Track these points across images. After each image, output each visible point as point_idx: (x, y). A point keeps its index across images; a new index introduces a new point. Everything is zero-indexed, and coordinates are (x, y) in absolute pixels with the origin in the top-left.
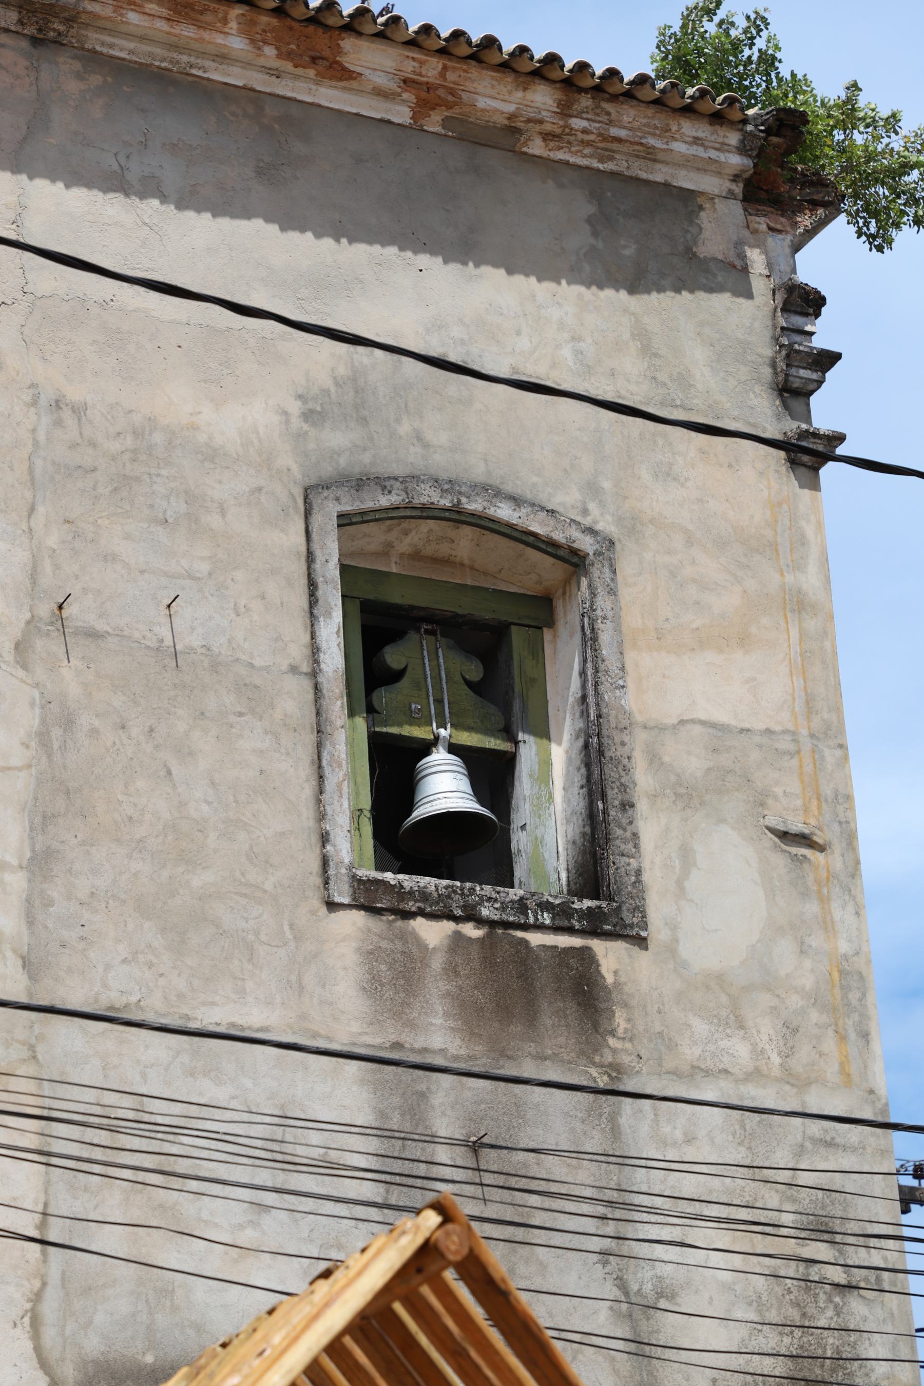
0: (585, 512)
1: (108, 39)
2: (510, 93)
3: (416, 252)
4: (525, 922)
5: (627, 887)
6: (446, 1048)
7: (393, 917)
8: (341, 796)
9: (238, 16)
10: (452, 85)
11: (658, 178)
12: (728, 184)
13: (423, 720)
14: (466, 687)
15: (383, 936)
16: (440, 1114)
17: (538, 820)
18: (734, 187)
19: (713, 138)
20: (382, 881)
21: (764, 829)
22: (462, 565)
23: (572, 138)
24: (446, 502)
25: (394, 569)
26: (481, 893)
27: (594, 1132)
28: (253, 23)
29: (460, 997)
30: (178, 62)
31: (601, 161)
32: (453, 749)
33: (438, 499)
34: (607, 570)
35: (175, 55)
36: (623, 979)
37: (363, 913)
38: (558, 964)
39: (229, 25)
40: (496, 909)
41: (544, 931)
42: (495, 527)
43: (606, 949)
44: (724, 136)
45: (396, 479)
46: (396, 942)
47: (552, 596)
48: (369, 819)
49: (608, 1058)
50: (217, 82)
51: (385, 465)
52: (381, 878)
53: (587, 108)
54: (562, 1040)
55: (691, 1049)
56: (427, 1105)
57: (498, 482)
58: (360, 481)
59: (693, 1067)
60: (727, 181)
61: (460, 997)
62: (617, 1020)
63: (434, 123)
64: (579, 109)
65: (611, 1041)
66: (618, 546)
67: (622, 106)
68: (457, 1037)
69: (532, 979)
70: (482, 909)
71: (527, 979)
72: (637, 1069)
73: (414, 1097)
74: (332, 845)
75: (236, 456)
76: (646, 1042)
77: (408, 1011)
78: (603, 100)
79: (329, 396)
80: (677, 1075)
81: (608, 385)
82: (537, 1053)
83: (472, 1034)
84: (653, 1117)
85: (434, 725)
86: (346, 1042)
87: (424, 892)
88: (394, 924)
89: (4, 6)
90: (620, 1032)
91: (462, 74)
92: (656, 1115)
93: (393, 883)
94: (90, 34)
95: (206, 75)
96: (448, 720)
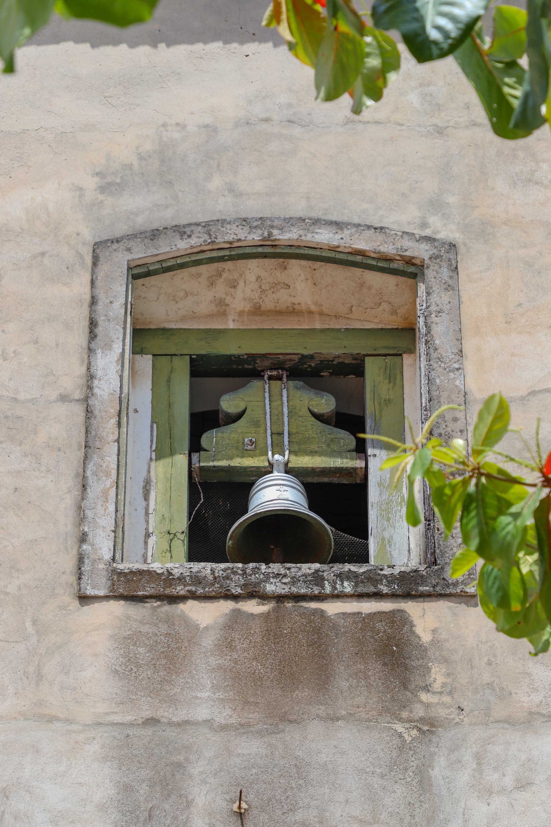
0: (424, 225)
3: (242, 43)
4: (320, 593)
5: (452, 549)
6: (213, 719)
7: (159, 603)
8: (107, 501)
13: (258, 451)
14: (313, 419)
15: (145, 621)
16: (199, 782)
17: (386, 523)
20: (148, 571)
22: (310, 312)
24: (256, 237)
25: (231, 326)
26: (267, 571)
27: (396, 786)
29: (234, 670)
32: (288, 471)
33: (246, 235)
34: (446, 270)
36: (444, 635)
37: (122, 602)
38: (361, 629)
40: (285, 584)
41: (346, 600)
42: (318, 253)
43: (424, 610)
45: (198, 224)
46: (160, 626)
48: (183, 541)
49: (419, 712)
51: (189, 216)
52: (146, 569)
54: (360, 700)
55: (529, 696)
56: (183, 774)
57: (320, 214)
58: (156, 232)
59: (531, 713)
61: (234, 670)
62: (433, 676)
65: (424, 696)
66: (462, 249)
68: (227, 707)
69: (326, 646)
70: (267, 585)
71: (320, 646)
72: (457, 720)
73: (168, 768)
74: (89, 544)
75: (20, 230)
76: (470, 694)
77: (168, 688)
79: (131, 169)
80: (509, 723)
81: (461, 117)
82: (327, 714)
83: (247, 703)
84: (475, 766)
85: (270, 453)
86: (89, 723)
87: (196, 577)
88: (159, 610)
90: (437, 687)
92: (478, 764)
93: (159, 571)
96: (287, 447)
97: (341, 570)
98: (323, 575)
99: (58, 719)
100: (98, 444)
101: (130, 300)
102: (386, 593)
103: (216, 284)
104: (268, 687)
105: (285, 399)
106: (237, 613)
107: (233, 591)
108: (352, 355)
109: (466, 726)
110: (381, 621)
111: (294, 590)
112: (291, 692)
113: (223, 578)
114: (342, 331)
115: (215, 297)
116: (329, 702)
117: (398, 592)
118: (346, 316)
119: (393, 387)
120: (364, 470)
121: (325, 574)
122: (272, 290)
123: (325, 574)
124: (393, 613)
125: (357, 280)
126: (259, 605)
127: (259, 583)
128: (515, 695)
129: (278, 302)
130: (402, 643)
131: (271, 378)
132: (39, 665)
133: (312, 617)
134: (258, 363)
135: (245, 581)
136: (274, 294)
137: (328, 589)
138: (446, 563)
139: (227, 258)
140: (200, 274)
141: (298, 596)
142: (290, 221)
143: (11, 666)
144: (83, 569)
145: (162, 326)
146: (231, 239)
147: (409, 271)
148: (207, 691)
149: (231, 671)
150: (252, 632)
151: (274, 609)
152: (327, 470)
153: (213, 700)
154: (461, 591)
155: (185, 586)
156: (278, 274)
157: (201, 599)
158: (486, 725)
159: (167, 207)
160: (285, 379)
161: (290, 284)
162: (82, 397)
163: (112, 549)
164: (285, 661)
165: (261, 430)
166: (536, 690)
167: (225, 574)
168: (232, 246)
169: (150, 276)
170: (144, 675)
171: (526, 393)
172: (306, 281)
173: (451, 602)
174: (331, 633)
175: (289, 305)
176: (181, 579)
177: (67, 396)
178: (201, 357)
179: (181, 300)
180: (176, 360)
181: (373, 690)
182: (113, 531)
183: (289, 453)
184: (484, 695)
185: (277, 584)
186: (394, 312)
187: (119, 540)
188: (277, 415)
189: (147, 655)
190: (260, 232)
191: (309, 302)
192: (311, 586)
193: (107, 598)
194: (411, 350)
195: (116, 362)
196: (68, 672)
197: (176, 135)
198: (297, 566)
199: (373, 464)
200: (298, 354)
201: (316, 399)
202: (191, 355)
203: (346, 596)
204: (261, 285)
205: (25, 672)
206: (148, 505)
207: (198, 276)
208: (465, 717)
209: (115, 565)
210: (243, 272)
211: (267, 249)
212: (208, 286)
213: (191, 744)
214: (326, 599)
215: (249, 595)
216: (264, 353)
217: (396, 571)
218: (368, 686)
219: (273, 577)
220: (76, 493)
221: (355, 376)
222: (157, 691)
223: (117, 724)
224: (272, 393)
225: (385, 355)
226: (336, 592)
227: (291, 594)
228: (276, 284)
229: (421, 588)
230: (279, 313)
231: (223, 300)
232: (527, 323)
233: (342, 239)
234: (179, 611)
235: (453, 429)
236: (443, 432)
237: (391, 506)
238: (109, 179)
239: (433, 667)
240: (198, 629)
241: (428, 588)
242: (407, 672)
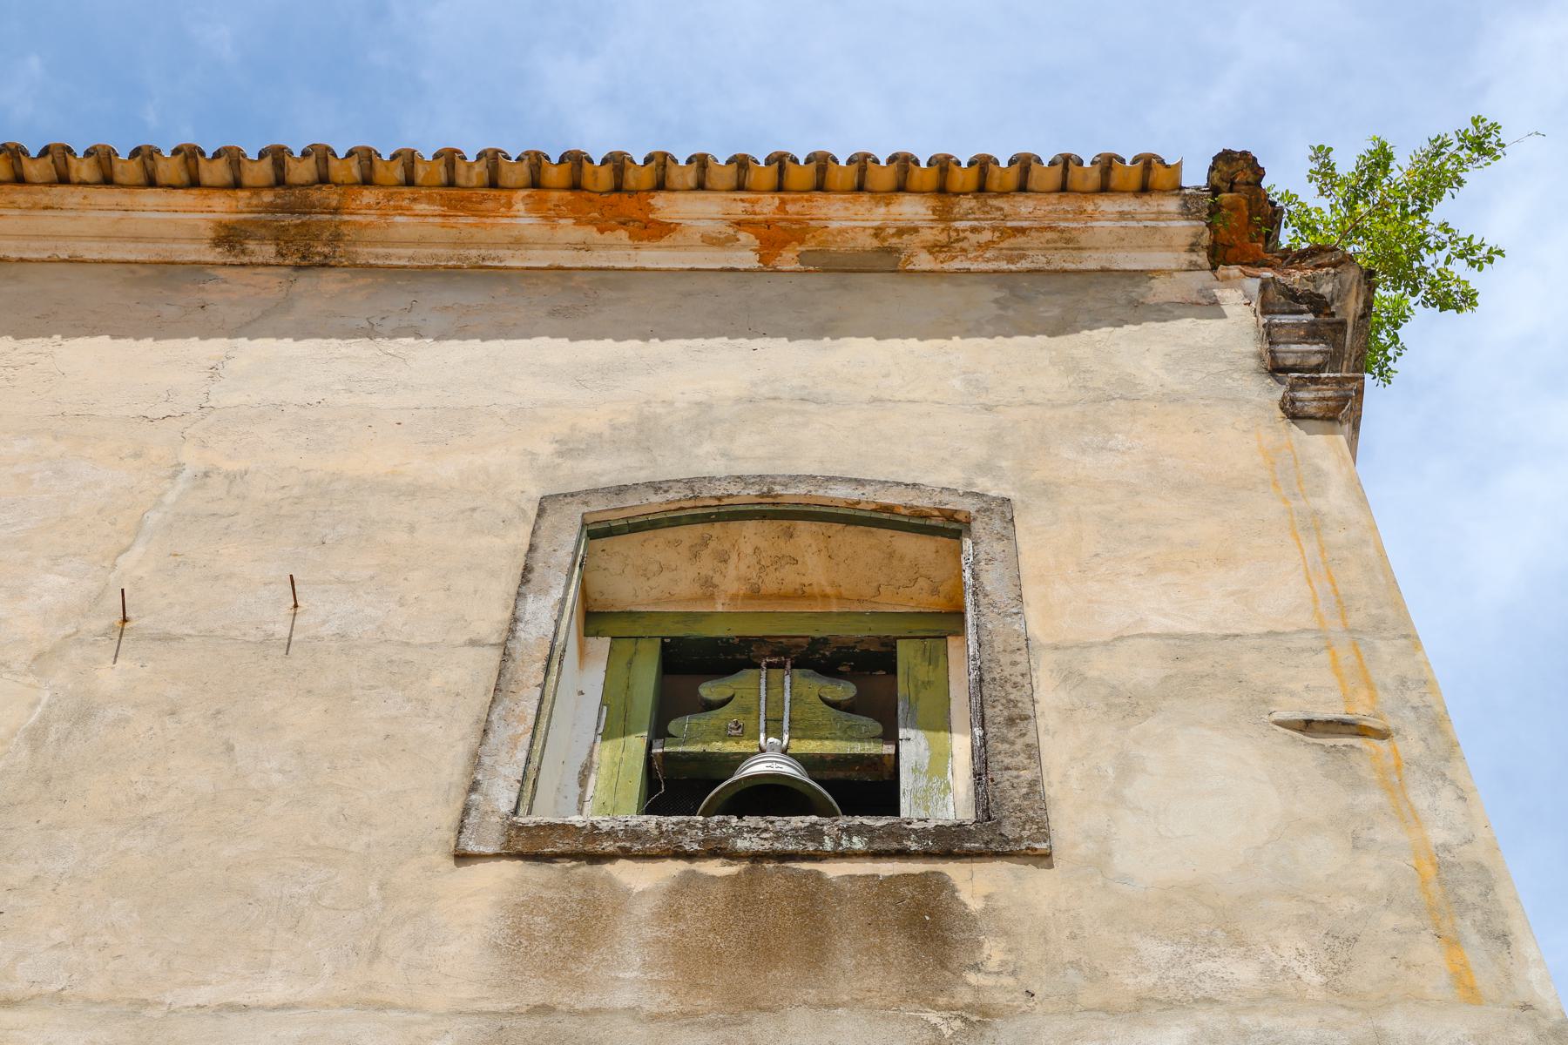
1: (381, 251)
2: (869, 210)
4: (816, 850)
5: (1012, 801)
6: (639, 1006)
7: (574, 863)
9: (523, 198)
10: (796, 217)
11: (1092, 265)
12: (1186, 257)
18: (1194, 257)
19: (1144, 209)
20: (564, 825)
21: (1271, 725)
22: (825, 596)
23: (964, 244)
25: (720, 609)
26: (740, 824)
28: (542, 201)
30: (467, 258)
31: (1010, 260)
35: (462, 252)
37: (519, 863)
38: (877, 894)
39: (515, 208)
40: (765, 839)
41: (855, 859)
44: (1158, 205)
46: (572, 890)
47: (963, 610)
49: (964, 996)
50: (517, 268)
53: (971, 209)
54: (874, 982)
59: (1140, 999)
60: (1183, 253)
62: (986, 952)
63: (788, 259)
64: (961, 211)
65: (972, 978)
66: (1018, 506)
67: (1016, 199)
72: (1024, 1008)
77: (574, 966)
78: (989, 197)
80: (1107, 1012)
85: (762, 736)
88: (573, 872)
89: (257, 242)
90: (992, 965)
91: (805, 204)
94: (359, 250)
95: (503, 264)
98: (822, 830)
99: (393, 1007)
100: (513, 687)
101: (581, 552)
102: (915, 850)
104: (730, 965)
105: (787, 685)
106: (689, 879)
107: (687, 848)
108: (879, 638)
110: (908, 885)
111: (778, 846)
112: (765, 972)
113: (674, 833)
116: (824, 984)
117: (933, 849)
118: (872, 599)
119: (934, 670)
120: (893, 758)
121: (825, 828)
122: (775, 567)
123: (825, 828)
124: (926, 875)
125: (885, 548)
127: (727, 839)
128: (1114, 976)
130: (939, 911)
131: (769, 666)
132: (378, 938)
133: (804, 880)
134: (753, 651)
137: (828, 845)
138: (1004, 817)
142: (796, 479)
143: (335, 940)
144: (466, 821)
145: (628, 609)
146: (720, 494)
147: (951, 527)
148: (634, 970)
149: (674, 945)
150: (711, 898)
151: (746, 871)
153: (642, 982)
154: (1028, 848)
155: (615, 842)
158: (1071, 1014)
159: (641, 469)
160: (788, 666)
162: (500, 641)
163: (515, 801)
164: (758, 933)
165: (753, 716)
166: (1146, 970)
167: (676, 828)
168: (722, 504)
169: (613, 535)
170: (539, 950)
171: (1111, 638)
173: (1012, 863)
174: (832, 899)
176: (611, 834)
177: (480, 641)
180: (642, 644)
181: (893, 969)
182: (518, 781)
183: (790, 738)
184: (1065, 976)
185: (753, 840)
186: (935, 591)
187: (527, 795)
188: (776, 702)
189: (547, 926)
190: (758, 488)
192: (804, 842)
194: (960, 631)
195: (552, 607)
196: (422, 947)
197: (660, 410)
199: (903, 747)
200: (808, 637)
201: (830, 686)
202: (663, 638)
203: (856, 854)
204: (760, 560)
205: (354, 947)
206: (584, 792)
208: (1036, 1004)
209: (515, 819)
210: (736, 541)
213: (601, 1039)
214: (826, 859)
217: (931, 825)
218: (886, 965)
219: (748, 832)
220: (474, 740)
221: (884, 673)
222: (556, 970)
223: (488, 1013)
224: (771, 680)
225: (924, 638)
226: (841, 848)
229: (967, 845)
230: (782, 597)
232: (1107, 572)
233: (863, 494)
234: (604, 872)
235: (1012, 673)
236: (997, 676)
237: (930, 793)
239: (986, 941)
240: (629, 895)
241: (977, 845)
242: (946, 947)
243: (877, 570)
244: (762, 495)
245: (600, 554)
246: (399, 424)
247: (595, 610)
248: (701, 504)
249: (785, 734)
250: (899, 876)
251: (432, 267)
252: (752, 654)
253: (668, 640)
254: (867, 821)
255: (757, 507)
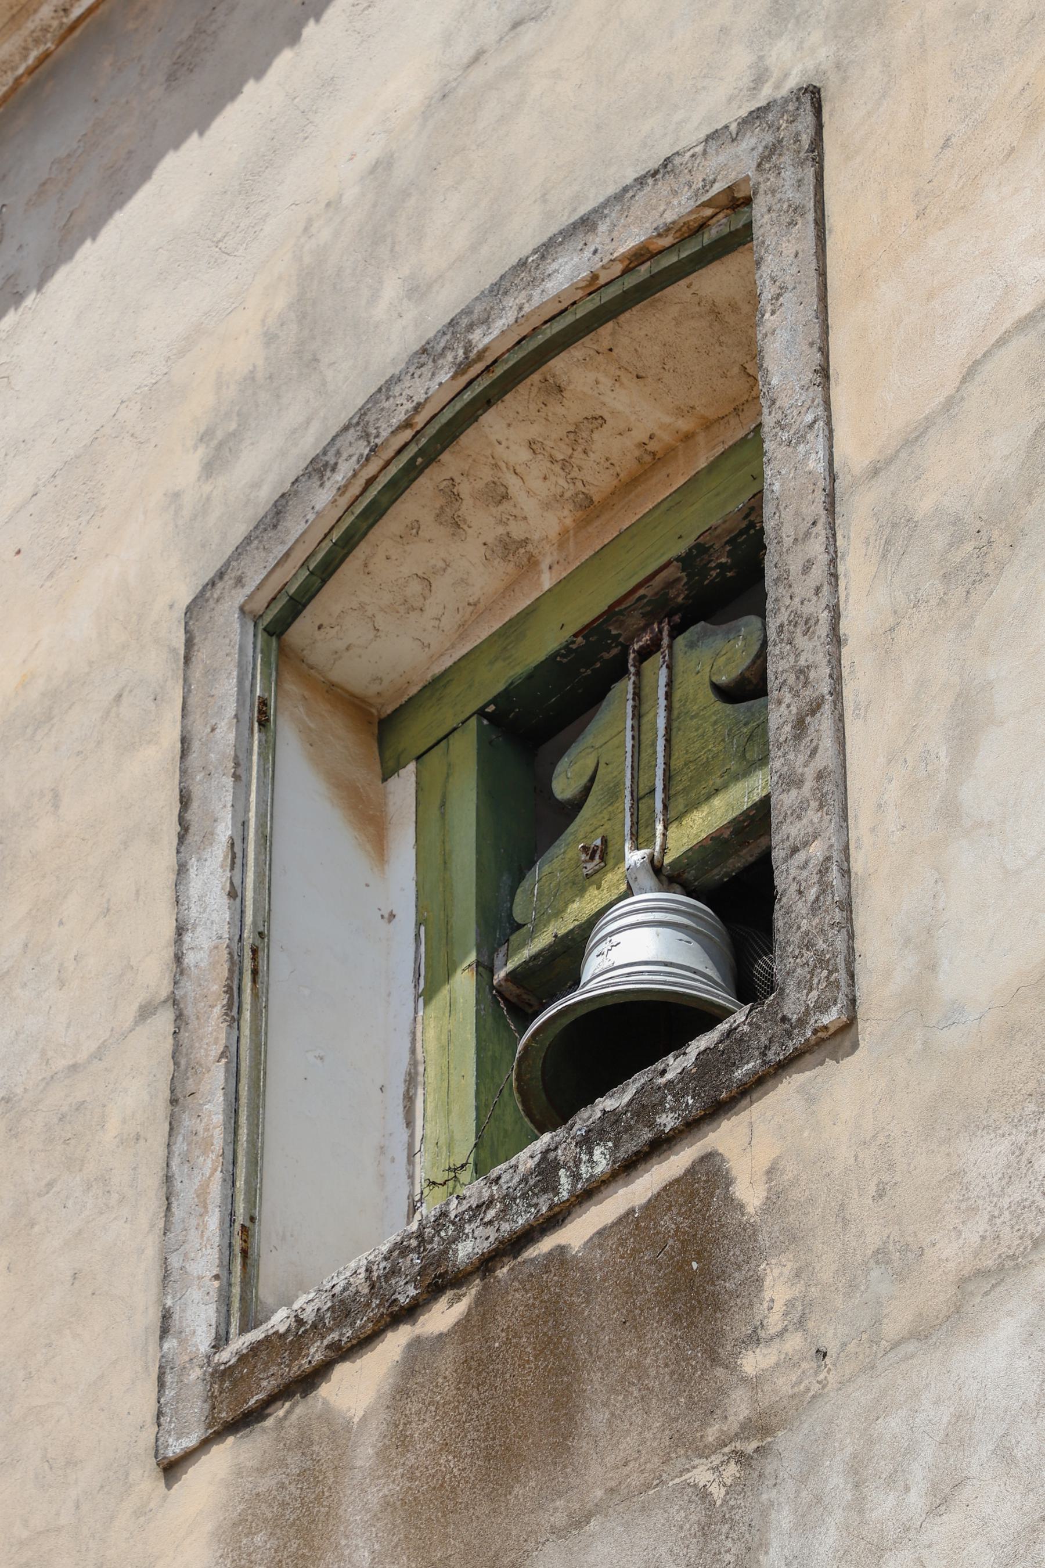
4: (550, 1208)
7: (287, 1405)
22: (688, 437)
30: (45, 30)
35: (30, 25)
37: (230, 1440)
41: (605, 1192)
72: (816, 1387)
93: (282, 1329)
97: (588, 1123)
103: (465, 521)
109: (831, 1394)
114: (751, 439)
115: (485, 544)
122: (580, 449)
126: (452, 1306)
129: (612, 464)
133: (545, 1277)
134: (619, 635)
135: (422, 1261)
136: (591, 454)
139: (420, 460)
140: (415, 524)
141: (519, 1238)
145: (429, 677)
146: (403, 417)
152: (744, 821)
154: (815, 1032)
156: (560, 410)
157: (357, 1352)
161: (599, 413)
168: (418, 428)
169: (305, 606)
172: (617, 384)
175: (637, 453)
177: (149, 1003)
178: (502, 697)
179: (425, 598)
191: (667, 419)
193: (205, 1444)
198: (511, 1164)
203: (603, 1182)
207: (414, 531)
210: (493, 458)
211: (479, 385)
212: (453, 534)
214: (569, 1214)
215: (433, 1291)
216: (606, 608)
227: (500, 1242)
228: (575, 432)
229: (738, 1074)
231: (508, 540)
238: (220, 434)
243: (718, 349)
244: (461, 369)
245: (319, 635)
246: (19, 552)
247: (389, 712)
248: (390, 452)
249: (657, 823)
250: (659, 1194)
251: (13, 89)
252: (621, 640)
253: (491, 708)
254: (608, 1103)
255: (467, 396)
